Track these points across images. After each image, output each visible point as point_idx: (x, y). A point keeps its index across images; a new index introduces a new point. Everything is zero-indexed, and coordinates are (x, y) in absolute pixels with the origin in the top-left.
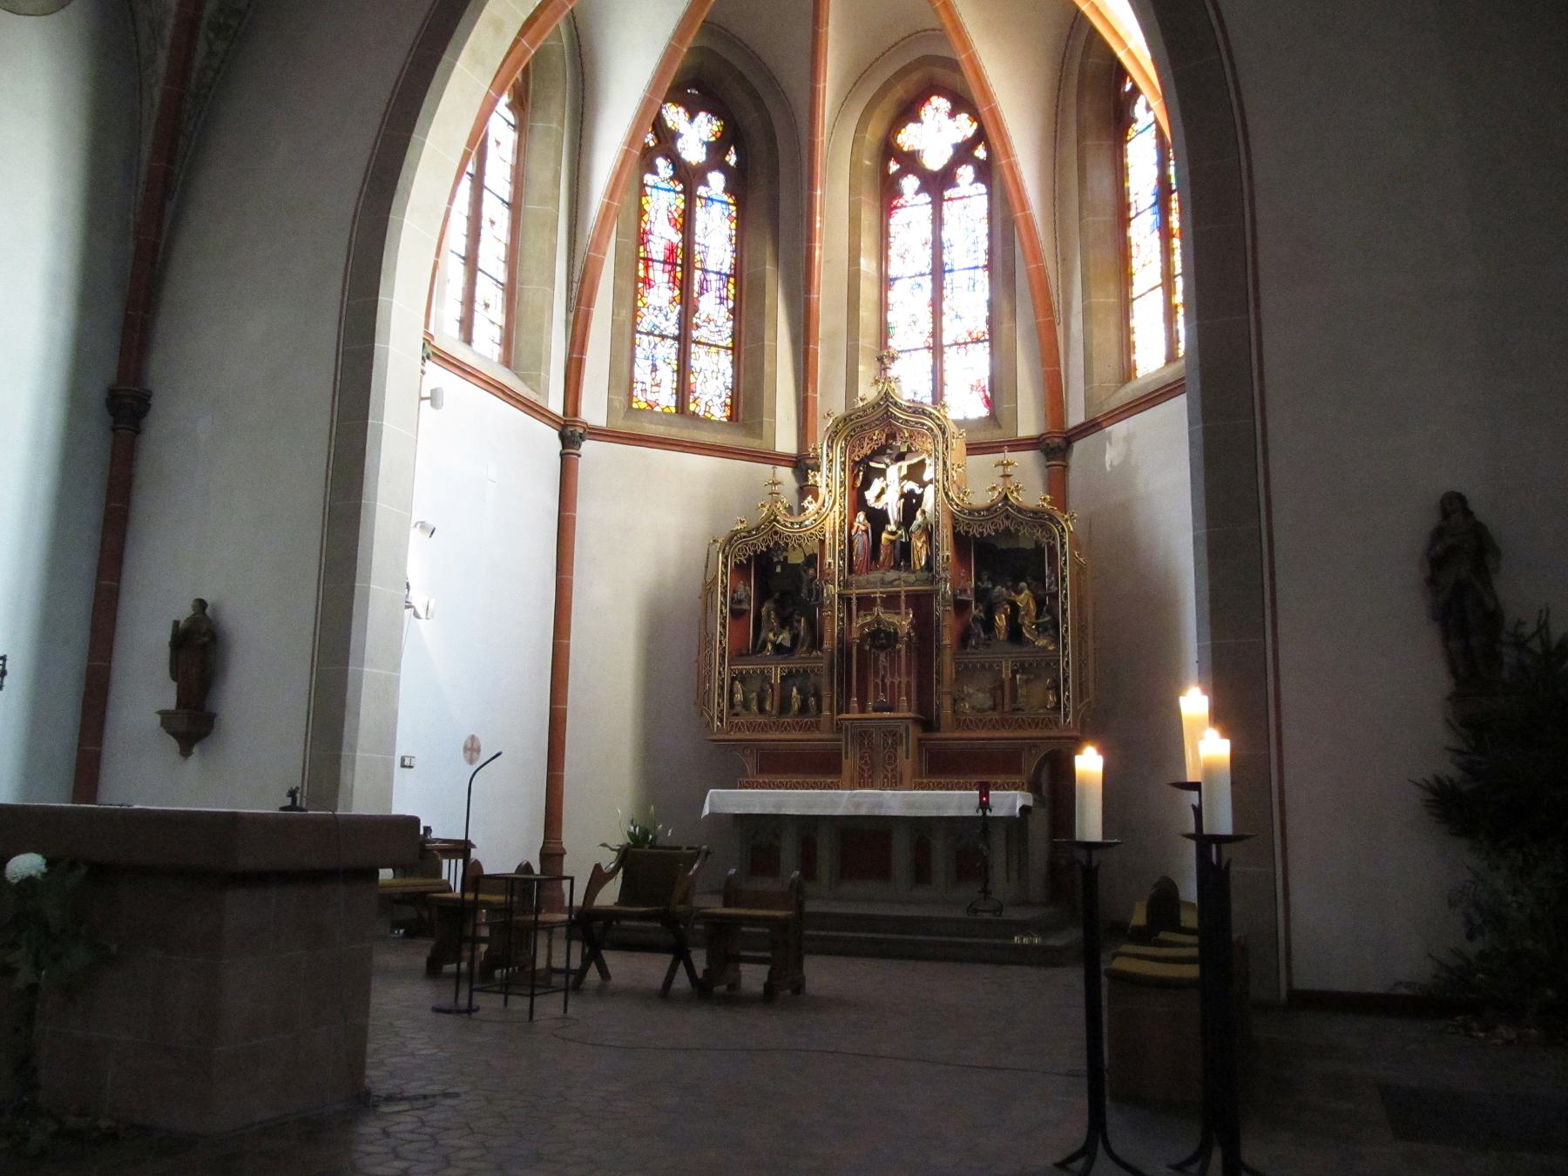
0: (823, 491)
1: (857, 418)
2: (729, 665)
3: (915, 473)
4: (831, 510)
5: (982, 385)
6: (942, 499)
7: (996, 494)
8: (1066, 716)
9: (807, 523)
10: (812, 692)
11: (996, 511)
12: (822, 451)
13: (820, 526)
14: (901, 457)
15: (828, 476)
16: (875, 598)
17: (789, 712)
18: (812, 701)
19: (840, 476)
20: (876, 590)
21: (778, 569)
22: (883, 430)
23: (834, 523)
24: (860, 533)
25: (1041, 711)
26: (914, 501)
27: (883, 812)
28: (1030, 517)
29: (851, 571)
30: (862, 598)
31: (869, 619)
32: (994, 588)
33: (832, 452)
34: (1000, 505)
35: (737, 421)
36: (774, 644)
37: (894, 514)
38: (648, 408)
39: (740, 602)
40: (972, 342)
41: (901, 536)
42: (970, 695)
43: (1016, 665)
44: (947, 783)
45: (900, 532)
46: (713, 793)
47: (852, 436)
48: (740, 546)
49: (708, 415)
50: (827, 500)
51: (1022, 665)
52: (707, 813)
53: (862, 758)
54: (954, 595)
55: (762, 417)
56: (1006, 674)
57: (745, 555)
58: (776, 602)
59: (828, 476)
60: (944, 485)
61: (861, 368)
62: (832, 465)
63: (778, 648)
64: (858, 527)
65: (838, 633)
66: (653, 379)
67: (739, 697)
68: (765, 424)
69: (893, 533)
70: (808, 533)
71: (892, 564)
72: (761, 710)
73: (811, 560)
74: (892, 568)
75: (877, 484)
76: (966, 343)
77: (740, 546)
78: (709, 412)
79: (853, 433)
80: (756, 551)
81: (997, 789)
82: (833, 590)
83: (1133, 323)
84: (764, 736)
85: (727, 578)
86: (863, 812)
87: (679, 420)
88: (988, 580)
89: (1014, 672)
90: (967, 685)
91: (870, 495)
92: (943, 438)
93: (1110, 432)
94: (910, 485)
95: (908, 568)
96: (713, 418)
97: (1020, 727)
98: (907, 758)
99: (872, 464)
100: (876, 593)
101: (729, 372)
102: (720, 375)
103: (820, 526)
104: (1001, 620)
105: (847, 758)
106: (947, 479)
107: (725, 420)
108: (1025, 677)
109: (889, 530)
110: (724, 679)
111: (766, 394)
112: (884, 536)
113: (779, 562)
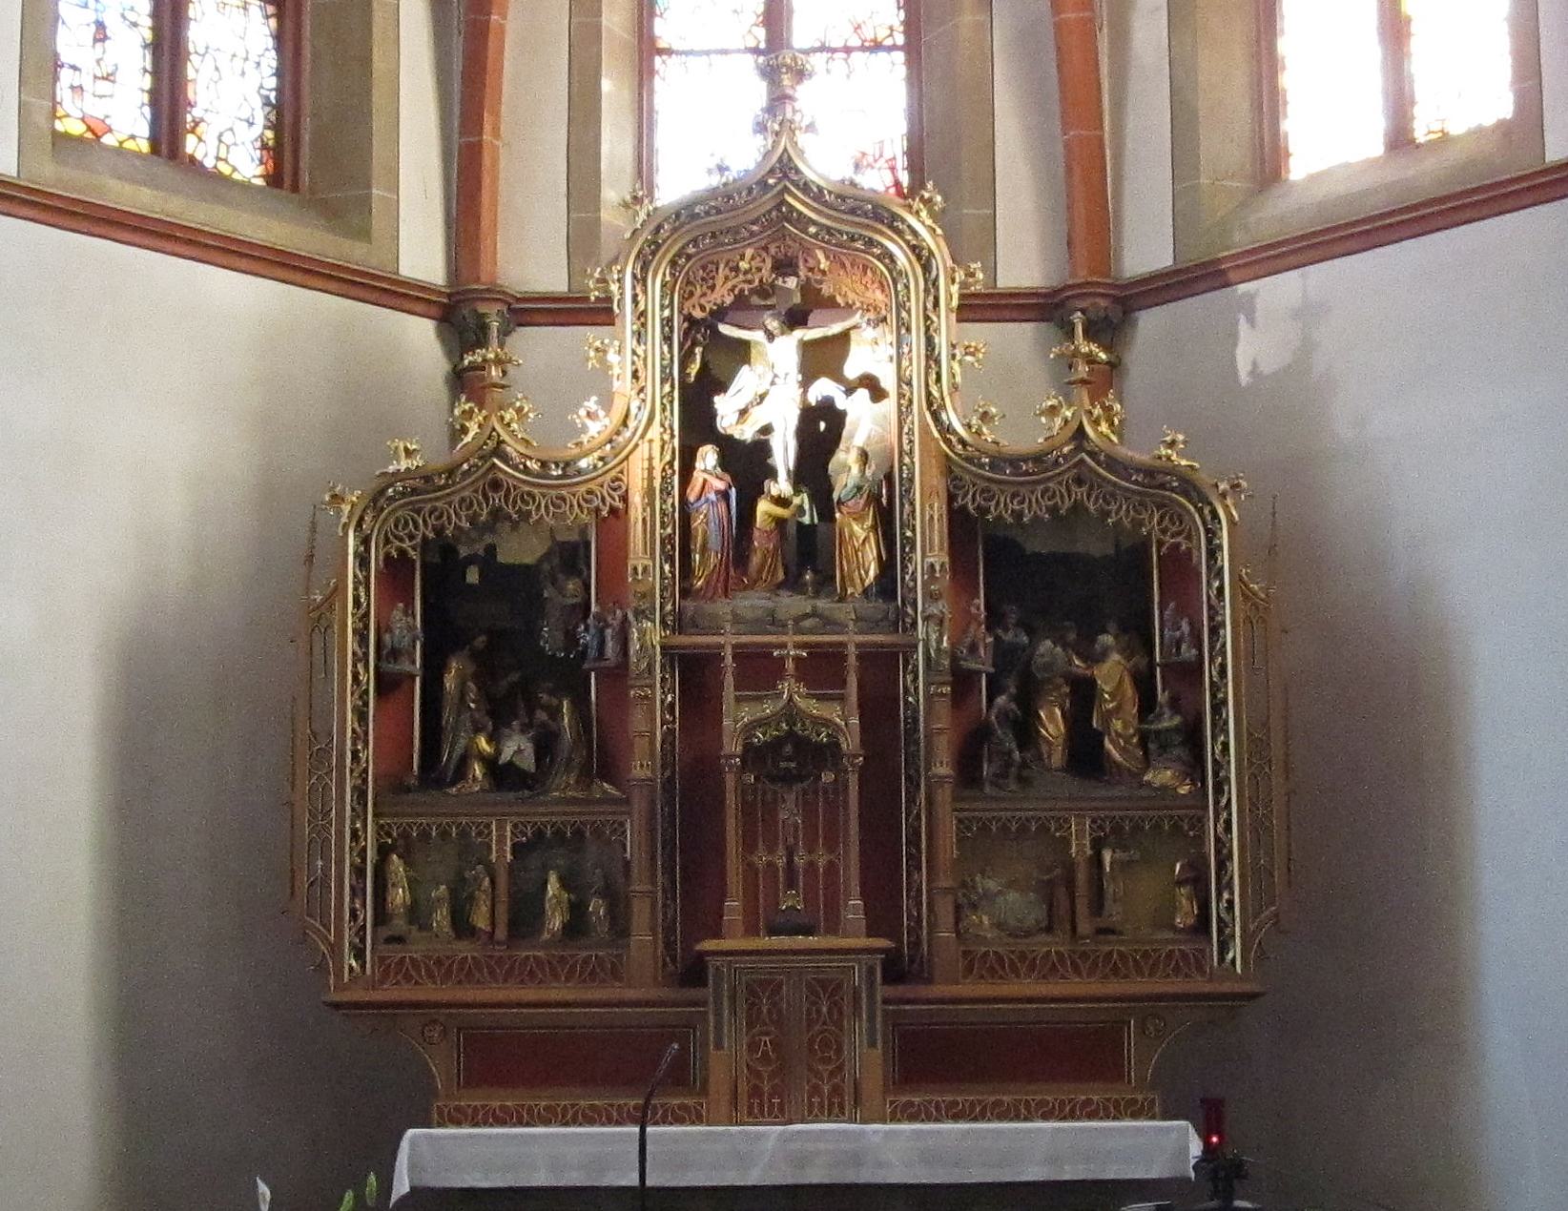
0: (623, 386)
1: (707, 213)
2: (375, 815)
3: (823, 358)
4: (642, 437)
5: (888, 155)
6: (925, 429)
7: (1058, 421)
8: (1223, 948)
9: (583, 464)
10: (599, 884)
11: (1056, 463)
12: (621, 288)
13: (618, 469)
14: (795, 319)
15: (634, 353)
16: (782, 659)
17: (540, 932)
18: (597, 907)
19: (662, 353)
20: (784, 638)
21: (473, 576)
22: (766, 249)
23: (651, 469)
24: (712, 496)
25: (1159, 936)
26: (822, 426)
27: (866, 1176)
28: (1136, 482)
29: (685, 593)
30: (749, 656)
31: (768, 709)
32: (1033, 644)
33: (645, 292)
34: (1066, 450)
35: (295, 188)
36: (491, 763)
37: (784, 452)
38: (89, 135)
39: (395, 654)
40: (863, 48)
41: (800, 509)
42: (987, 896)
43: (1101, 828)
44: (1062, 1103)
45: (796, 501)
46: (414, 1136)
47: (689, 257)
48: (399, 513)
49: (225, 169)
50: (634, 411)
51: (1117, 829)
52: (405, 1189)
53: (753, 1047)
54: (955, 659)
55: (369, 187)
56: (1079, 848)
57: (411, 537)
58: (475, 656)
59: (634, 353)
60: (929, 394)
61: (606, 85)
62: (644, 325)
63: (502, 775)
64: (705, 481)
65: (663, 742)
66: (98, 62)
67: (399, 896)
68: (376, 207)
69: (782, 501)
70: (583, 489)
71: (781, 576)
72: (462, 926)
73: (570, 556)
74: (780, 586)
75: (746, 382)
76: (848, 50)
77: (399, 513)
78: (226, 160)
79: (691, 250)
80: (443, 527)
81: (664, 1122)
82: (649, 635)
83: (1284, 46)
84: (470, 994)
85: (368, 595)
86: (815, 1176)
87: (162, 169)
88: (1017, 625)
89: (1098, 845)
90: (983, 873)
91: (726, 408)
92: (926, 281)
93: (1251, 297)
94: (823, 388)
95: (825, 582)
96: (236, 176)
97: (1115, 971)
98: (872, 1044)
99: (725, 329)
100: (783, 646)
101: (271, 60)
102: (250, 66)
103: (613, 473)
104: (1052, 723)
105: (719, 1046)
106: (939, 380)
107: (260, 182)
108: (1119, 854)
109: (774, 492)
110: (364, 849)
111: (378, 123)
112: (763, 507)
113: (471, 560)
